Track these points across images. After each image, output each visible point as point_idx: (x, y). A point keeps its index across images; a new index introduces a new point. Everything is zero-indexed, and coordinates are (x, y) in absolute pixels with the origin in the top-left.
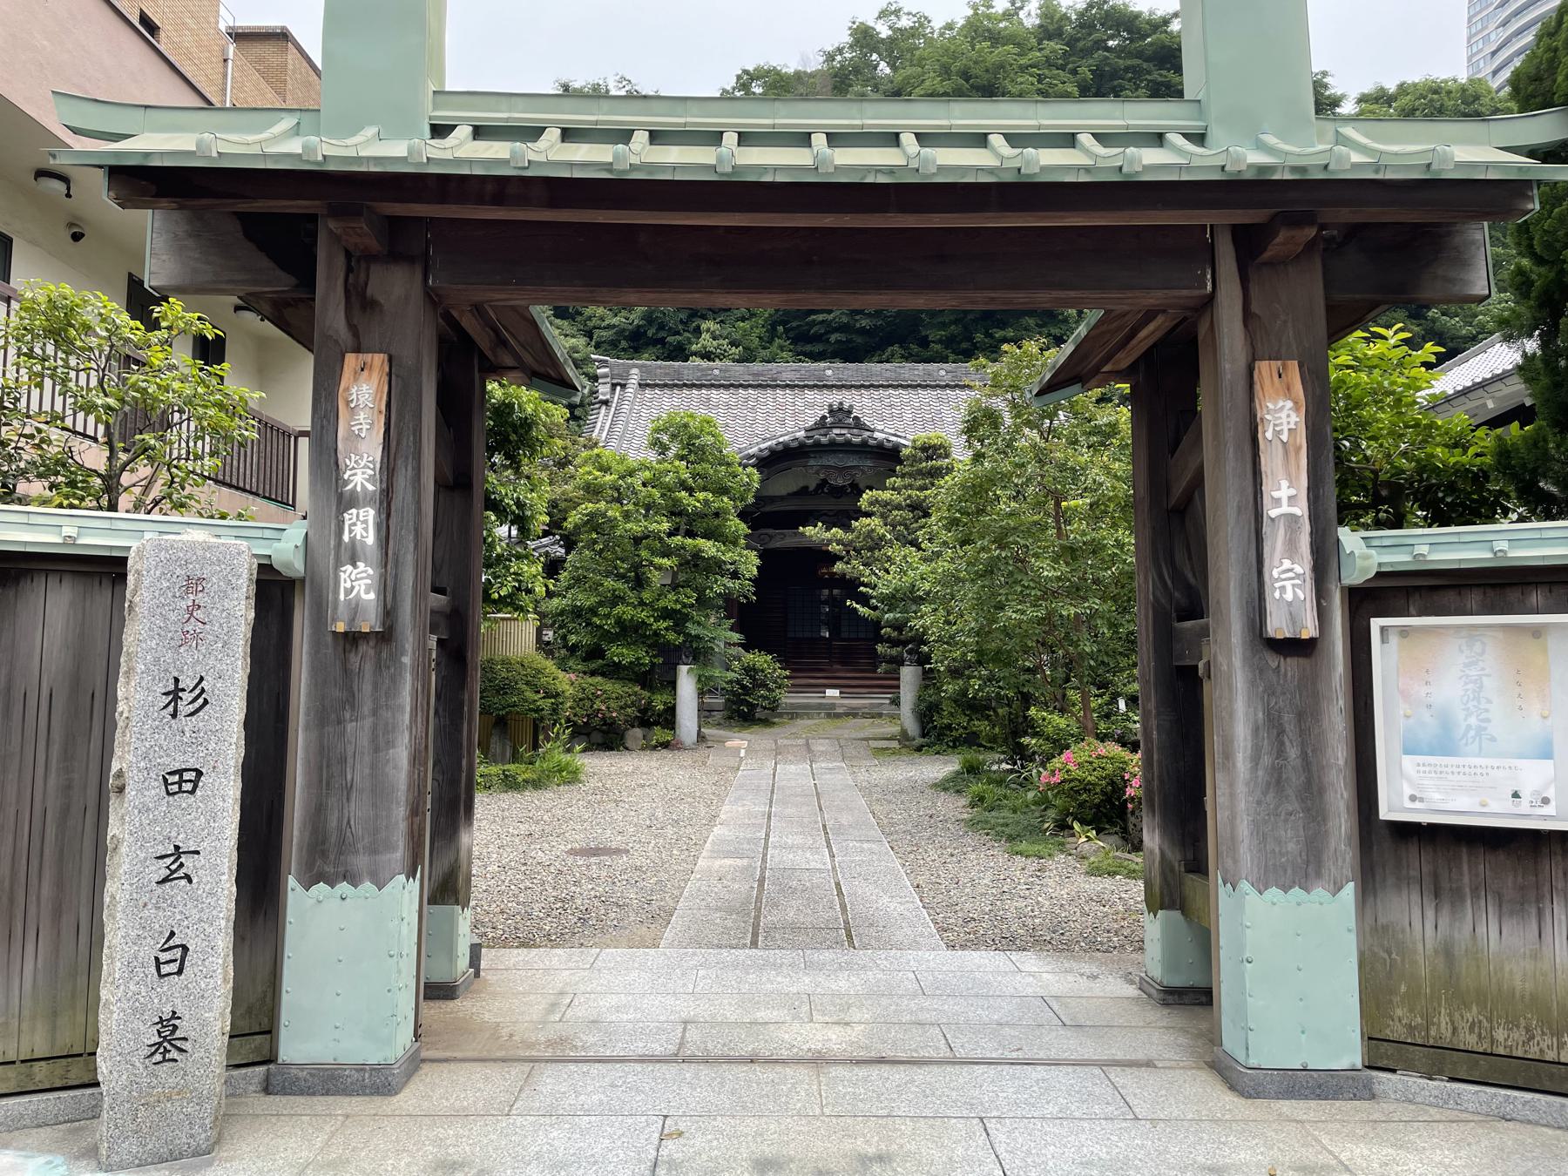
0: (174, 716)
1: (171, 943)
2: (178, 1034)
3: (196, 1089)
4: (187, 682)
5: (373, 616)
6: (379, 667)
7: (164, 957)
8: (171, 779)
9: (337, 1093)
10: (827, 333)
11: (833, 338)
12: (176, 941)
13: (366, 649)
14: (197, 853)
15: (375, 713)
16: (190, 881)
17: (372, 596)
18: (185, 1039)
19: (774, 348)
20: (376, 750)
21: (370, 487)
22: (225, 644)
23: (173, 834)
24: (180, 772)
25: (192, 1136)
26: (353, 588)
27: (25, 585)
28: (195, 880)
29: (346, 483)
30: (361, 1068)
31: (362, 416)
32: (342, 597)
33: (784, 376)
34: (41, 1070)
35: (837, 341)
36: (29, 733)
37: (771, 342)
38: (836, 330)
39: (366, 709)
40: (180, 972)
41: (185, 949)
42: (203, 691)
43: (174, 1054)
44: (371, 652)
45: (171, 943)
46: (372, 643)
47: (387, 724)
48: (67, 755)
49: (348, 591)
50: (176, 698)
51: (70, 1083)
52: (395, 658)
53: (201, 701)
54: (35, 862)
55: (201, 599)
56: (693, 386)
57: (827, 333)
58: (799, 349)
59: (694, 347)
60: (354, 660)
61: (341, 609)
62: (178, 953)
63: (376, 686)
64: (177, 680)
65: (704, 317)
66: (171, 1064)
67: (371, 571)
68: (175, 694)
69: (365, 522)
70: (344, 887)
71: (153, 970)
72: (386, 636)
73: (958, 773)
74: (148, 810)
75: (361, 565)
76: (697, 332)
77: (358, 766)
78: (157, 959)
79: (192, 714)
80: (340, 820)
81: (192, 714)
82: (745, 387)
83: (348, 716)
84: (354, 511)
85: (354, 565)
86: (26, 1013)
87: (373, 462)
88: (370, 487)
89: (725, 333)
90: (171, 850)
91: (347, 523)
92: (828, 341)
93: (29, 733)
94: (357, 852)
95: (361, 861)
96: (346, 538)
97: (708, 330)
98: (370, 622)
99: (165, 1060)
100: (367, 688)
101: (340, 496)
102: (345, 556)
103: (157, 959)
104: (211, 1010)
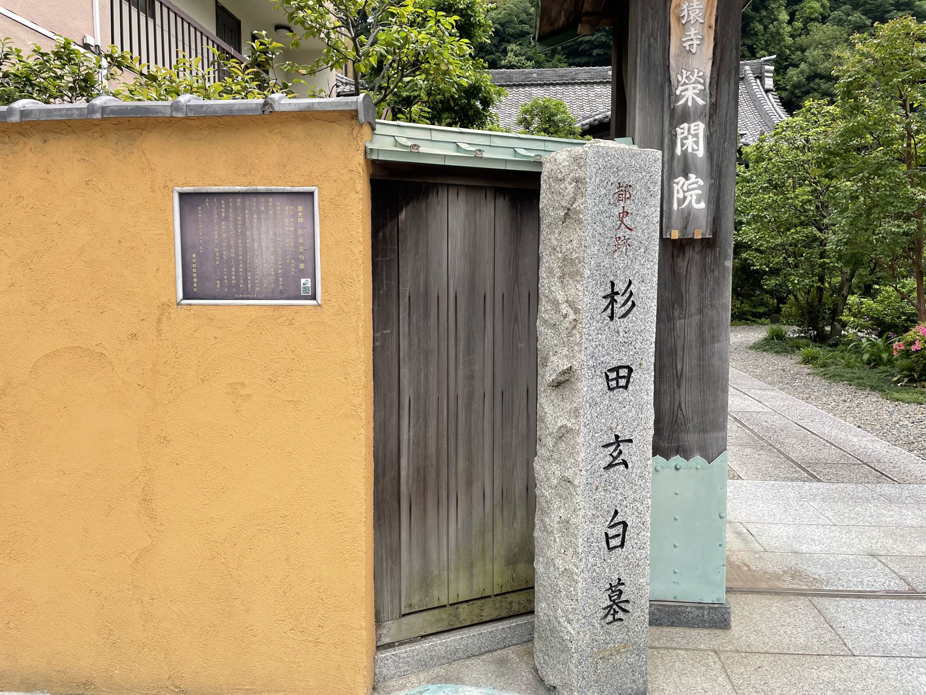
0: (612, 318)
1: (616, 521)
2: (623, 598)
3: (636, 643)
4: (620, 287)
5: (704, 224)
6: (703, 272)
7: (612, 532)
8: (613, 375)
9: (681, 624)
10: (591, 49)
11: (595, 52)
12: (619, 519)
13: (692, 254)
14: (630, 441)
15: (701, 311)
16: (627, 467)
17: (702, 205)
18: (627, 601)
19: (555, 61)
20: (703, 343)
21: (701, 102)
22: (646, 249)
23: (614, 425)
24: (616, 369)
25: (634, 681)
26: (685, 198)
27: (433, 199)
28: (630, 465)
29: (678, 98)
30: (700, 606)
31: (693, 31)
32: (675, 207)
33: (580, 76)
34: (463, 610)
35: (598, 55)
36: (443, 331)
37: (552, 57)
38: (596, 47)
39: (694, 307)
40: (622, 545)
41: (625, 525)
42: (631, 294)
43: (620, 615)
44: (697, 257)
45: (616, 521)
46: (697, 249)
47: (712, 321)
48: (469, 351)
49: (681, 201)
50: (613, 301)
51: (485, 619)
52: (718, 263)
53: (630, 303)
54: (452, 441)
55: (630, 206)
56: (520, 85)
57: (591, 49)
58: (571, 61)
59: (503, 62)
60: (682, 264)
61: (674, 218)
62: (620, 529)
63: (701, 287)
64: (613, 284)
65: (509, 42)
66: (619, 623)
67: (701, 182)
68: (612, 297)
69: (696, 136)
70: (677, 460)
71: (604, 544)
72: (709, 244)
73: (766, 339)
74: (596, 404)
75: (692, 176)
76: (505, 52)
77: (687, 359)
78: (606, 534)
79: (624, 316)
80: (672, 403)
81: (624, 316)
82: (554, 85)
83: (676, 313)
84: (685, 125)
85: (686, 177)
86: (452, 566)
87: (703, 77)
88: (701, 102)
89: (523, 52)
90: (613, 440)
91: (679, 137)
92: (591, 55)
93: (443, 331)
94: (688, 431)
95: (691, 439)
96: (678, 151)
97: (512, 51)
98: (700, 232)
99: (615, 620)
100: (694, 289)
101: (673, 111)
102: (677, 166)
103: (606, 534)
104: (644, 576)
